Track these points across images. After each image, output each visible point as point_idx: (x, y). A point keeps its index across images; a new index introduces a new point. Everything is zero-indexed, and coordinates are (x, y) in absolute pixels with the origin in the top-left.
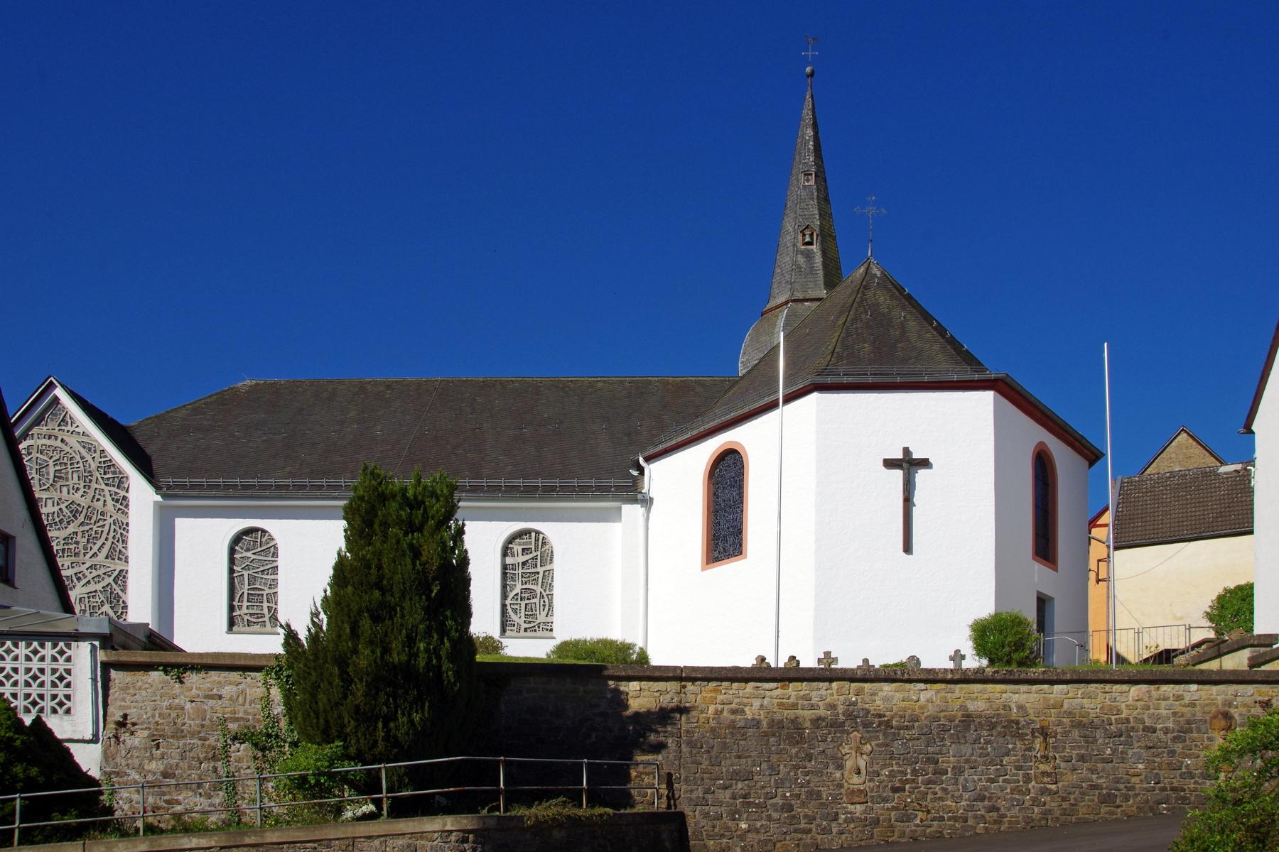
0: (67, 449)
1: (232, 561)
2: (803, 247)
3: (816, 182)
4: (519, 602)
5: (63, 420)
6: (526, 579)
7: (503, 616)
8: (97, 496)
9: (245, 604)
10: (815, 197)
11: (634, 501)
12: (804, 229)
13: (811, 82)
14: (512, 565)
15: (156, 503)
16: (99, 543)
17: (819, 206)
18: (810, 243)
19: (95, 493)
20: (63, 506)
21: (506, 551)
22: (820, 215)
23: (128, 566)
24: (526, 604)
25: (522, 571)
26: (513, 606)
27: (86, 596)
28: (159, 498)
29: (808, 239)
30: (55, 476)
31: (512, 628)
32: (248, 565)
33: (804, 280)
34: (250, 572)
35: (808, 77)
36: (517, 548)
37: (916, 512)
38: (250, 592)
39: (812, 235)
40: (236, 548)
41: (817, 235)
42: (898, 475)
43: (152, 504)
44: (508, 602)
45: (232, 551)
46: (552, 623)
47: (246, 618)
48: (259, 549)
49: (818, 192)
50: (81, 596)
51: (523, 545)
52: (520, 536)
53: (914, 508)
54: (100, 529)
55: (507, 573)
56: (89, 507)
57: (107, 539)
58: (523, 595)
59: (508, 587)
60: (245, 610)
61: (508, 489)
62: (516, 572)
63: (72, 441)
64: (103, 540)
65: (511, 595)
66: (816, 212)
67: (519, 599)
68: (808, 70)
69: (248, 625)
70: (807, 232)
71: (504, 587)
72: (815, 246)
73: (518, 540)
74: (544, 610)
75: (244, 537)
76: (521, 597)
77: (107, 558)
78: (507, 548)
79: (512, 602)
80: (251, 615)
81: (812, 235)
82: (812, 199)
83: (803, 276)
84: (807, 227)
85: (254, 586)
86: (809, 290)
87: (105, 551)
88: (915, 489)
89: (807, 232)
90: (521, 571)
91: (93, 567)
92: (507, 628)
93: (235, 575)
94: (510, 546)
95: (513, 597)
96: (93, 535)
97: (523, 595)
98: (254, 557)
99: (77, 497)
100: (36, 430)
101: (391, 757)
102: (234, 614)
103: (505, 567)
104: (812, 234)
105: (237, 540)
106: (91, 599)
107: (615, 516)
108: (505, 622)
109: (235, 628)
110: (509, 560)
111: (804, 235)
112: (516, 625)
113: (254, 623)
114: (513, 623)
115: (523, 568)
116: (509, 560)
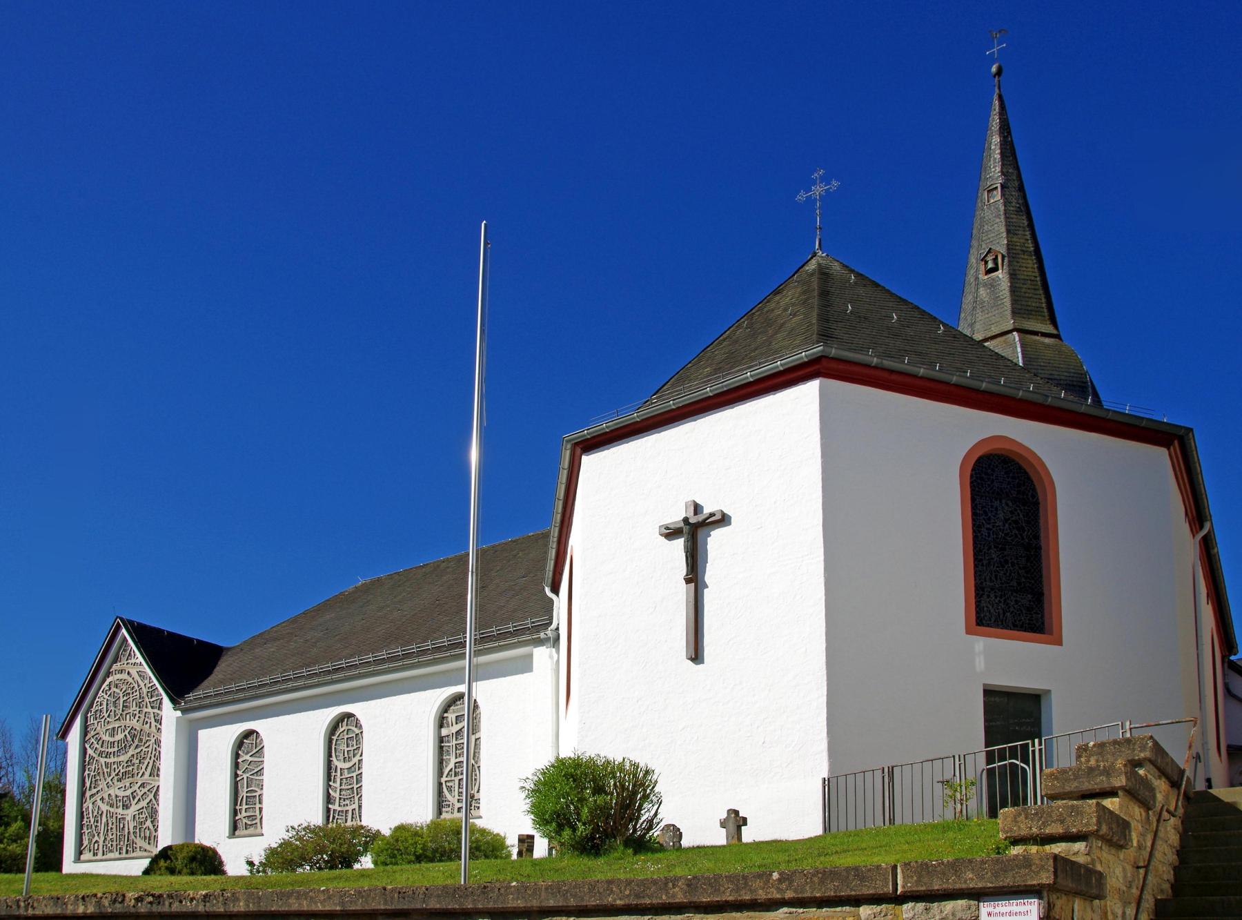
0: (130, 680)
1: (236, 765)
2: (986, 277)
3: (1003, 195)
4: (453, 778)
5: (130, 654)
6: (460, 751)
7: (440, 796)
8: (146, 720)
9: (244, 807)
10: (1002, 213)
11: (540, 642)
12: (986, 255)
13: (999, 81)
14: (447, 736)
15: (178, 718)
16: (146, 763)
17: (1006, 222)
18: (995, 269)
19: (145, 716)
20: (126, 733)
21: (441, 722)
22: (1008, 232)
23: (159, 781)
24: (460, 780)
25: (457, 742)
26: (448, 784)
27: (137, 813)
28: (179, 713)
29: (990, 265)
30: (123, 706)
31: (447, 809)
32: (247, 768)
33: (987, 316)
34: (248, 775)
35: (995, 77)
36: (451, 716)
37: (708, 596)
38: (248, 795)
39: (995, 260)
40: (240, 752)
41: (1003, 257)
42: (679, 544)
43: (175, 720)
44: (443, 780)
45: (236, 756)
46: (479, 799)
47: (244, 821)
48: (255, 751)
49: (1005, 206)
50: (135, 813)
51: (457, 712)
52: (455, 702)
53: (706, 590)
54: (147, 750)
55: (443, 746)
56: (142, 730)
57: (150, 759)
58: (457, 770)
59: (444, 763)
60: (244, 814)
61: (420, 653)
62: (451, 744)
63: (134, 672)
64: (148, 760)
65: (446, 772)
66: (1003, 229)
67: (453, 775)
68: (994, 69)
69: (246, 829)
70: (990, 258)
71: (440, 763)
72: (1000, 271)
73: (452, 708)
74: (475, 784)
75: (245, 741)
76: (455, 772)
77: (150, 776)
78: (443, 718)
79: (447, 779)
80: (249, 817)
81: (995, 260)
82: (998, 216)
83: (986, 311)
84: (989, 252)
85: (251, 789)
86: (992, 326)
87: (147, 774)
88: (706, 562)
89: (990, 258)
90: (454, 742)
91: (143, 785)
92: (444, 809)
93: (238, 779)
94: (446, 715)
95: (448, 774)
96: (143, 756)
97: (457, 770)
98: (251, 759)
99: (134, 723)
100: (114, 667)
101: (1151, 794)
102: (237, 818)
103: (441, 739)
104: (997, 257)
105: (240, 744)
106: (141, 816)
107: (525, 665)
108: (441, 801)
109: (237, 833)
110: (444, 732)
111: (986, 263)
112: (451, 805)
113: (251, 825)
114: (448, 803)
115: (456, 739)
116: (444, 732)
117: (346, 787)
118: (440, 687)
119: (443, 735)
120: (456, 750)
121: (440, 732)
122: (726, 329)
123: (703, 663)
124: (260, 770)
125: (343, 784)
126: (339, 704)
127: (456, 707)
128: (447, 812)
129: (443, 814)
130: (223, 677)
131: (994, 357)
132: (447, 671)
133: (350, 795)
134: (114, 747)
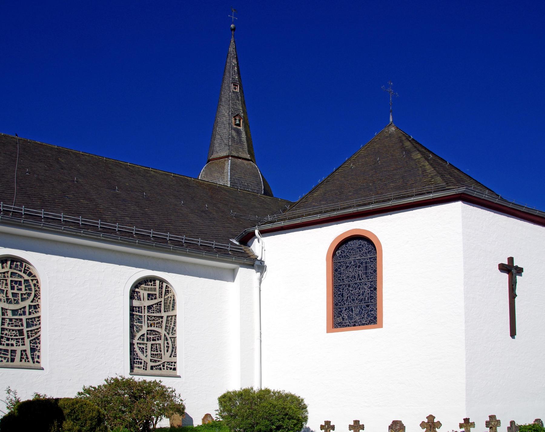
4: (145, 342)
6: (151, 322)
21: (133, 295)
25: (149, 314)
52: (145, 282)
62: (143, 314)
73: (143, 286)
79: (139, 342)
95: (140, 338)
112: (143, 363)
114: (140, 361)
117: (10, 327)
118: (137, 266)
119: (134, 305)
120: (148, 320)
121: (131, 303)
122: (473, 178)
123: (382, 328)
124: (37, 329)
125: (6, 324)
126: (153, 269)
127: (146, 286)
128: (139, 367)
129: (135, 369)
130: (314, 195)
131: (88, 188)
132: (149, 257)
133: (16, 336)
134: (161, 297)
